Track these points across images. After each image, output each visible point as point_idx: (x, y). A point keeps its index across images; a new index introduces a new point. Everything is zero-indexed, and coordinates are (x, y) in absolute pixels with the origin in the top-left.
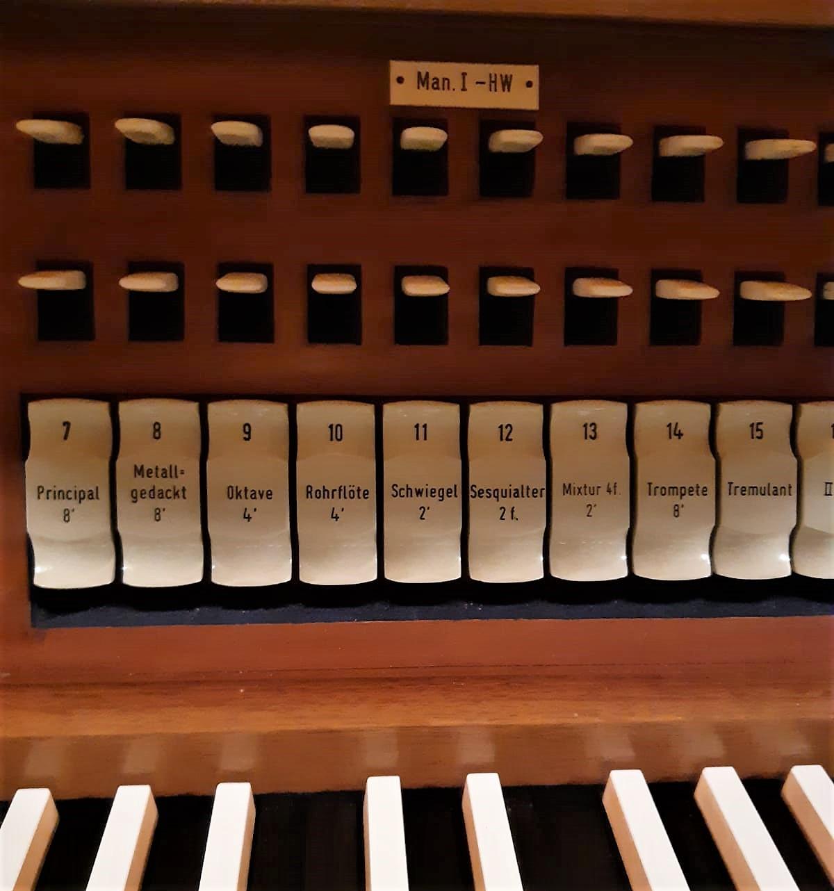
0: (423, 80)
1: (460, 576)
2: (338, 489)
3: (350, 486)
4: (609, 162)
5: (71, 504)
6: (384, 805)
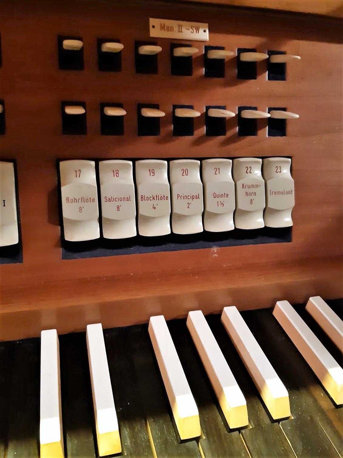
0: (163, 27)
1: (104, 237)
2: (81, 198)
3: (86, 197)
4: (115, 56)
5: (190, 201)
6: (50, 343)
